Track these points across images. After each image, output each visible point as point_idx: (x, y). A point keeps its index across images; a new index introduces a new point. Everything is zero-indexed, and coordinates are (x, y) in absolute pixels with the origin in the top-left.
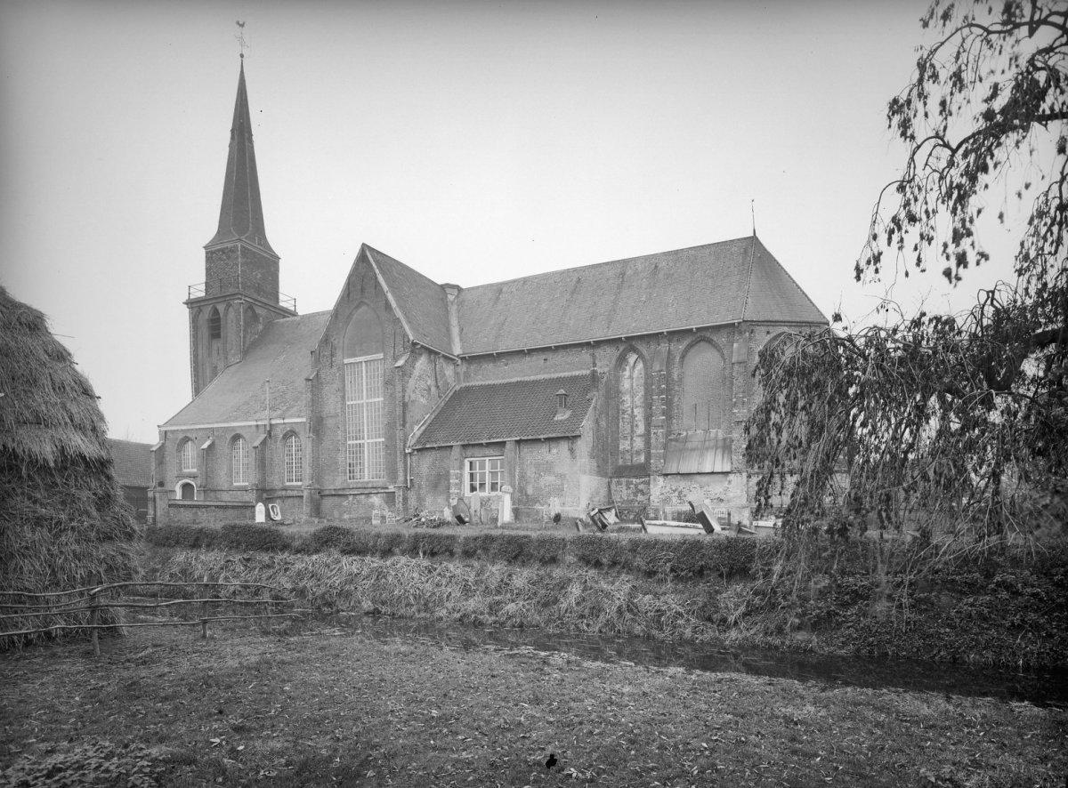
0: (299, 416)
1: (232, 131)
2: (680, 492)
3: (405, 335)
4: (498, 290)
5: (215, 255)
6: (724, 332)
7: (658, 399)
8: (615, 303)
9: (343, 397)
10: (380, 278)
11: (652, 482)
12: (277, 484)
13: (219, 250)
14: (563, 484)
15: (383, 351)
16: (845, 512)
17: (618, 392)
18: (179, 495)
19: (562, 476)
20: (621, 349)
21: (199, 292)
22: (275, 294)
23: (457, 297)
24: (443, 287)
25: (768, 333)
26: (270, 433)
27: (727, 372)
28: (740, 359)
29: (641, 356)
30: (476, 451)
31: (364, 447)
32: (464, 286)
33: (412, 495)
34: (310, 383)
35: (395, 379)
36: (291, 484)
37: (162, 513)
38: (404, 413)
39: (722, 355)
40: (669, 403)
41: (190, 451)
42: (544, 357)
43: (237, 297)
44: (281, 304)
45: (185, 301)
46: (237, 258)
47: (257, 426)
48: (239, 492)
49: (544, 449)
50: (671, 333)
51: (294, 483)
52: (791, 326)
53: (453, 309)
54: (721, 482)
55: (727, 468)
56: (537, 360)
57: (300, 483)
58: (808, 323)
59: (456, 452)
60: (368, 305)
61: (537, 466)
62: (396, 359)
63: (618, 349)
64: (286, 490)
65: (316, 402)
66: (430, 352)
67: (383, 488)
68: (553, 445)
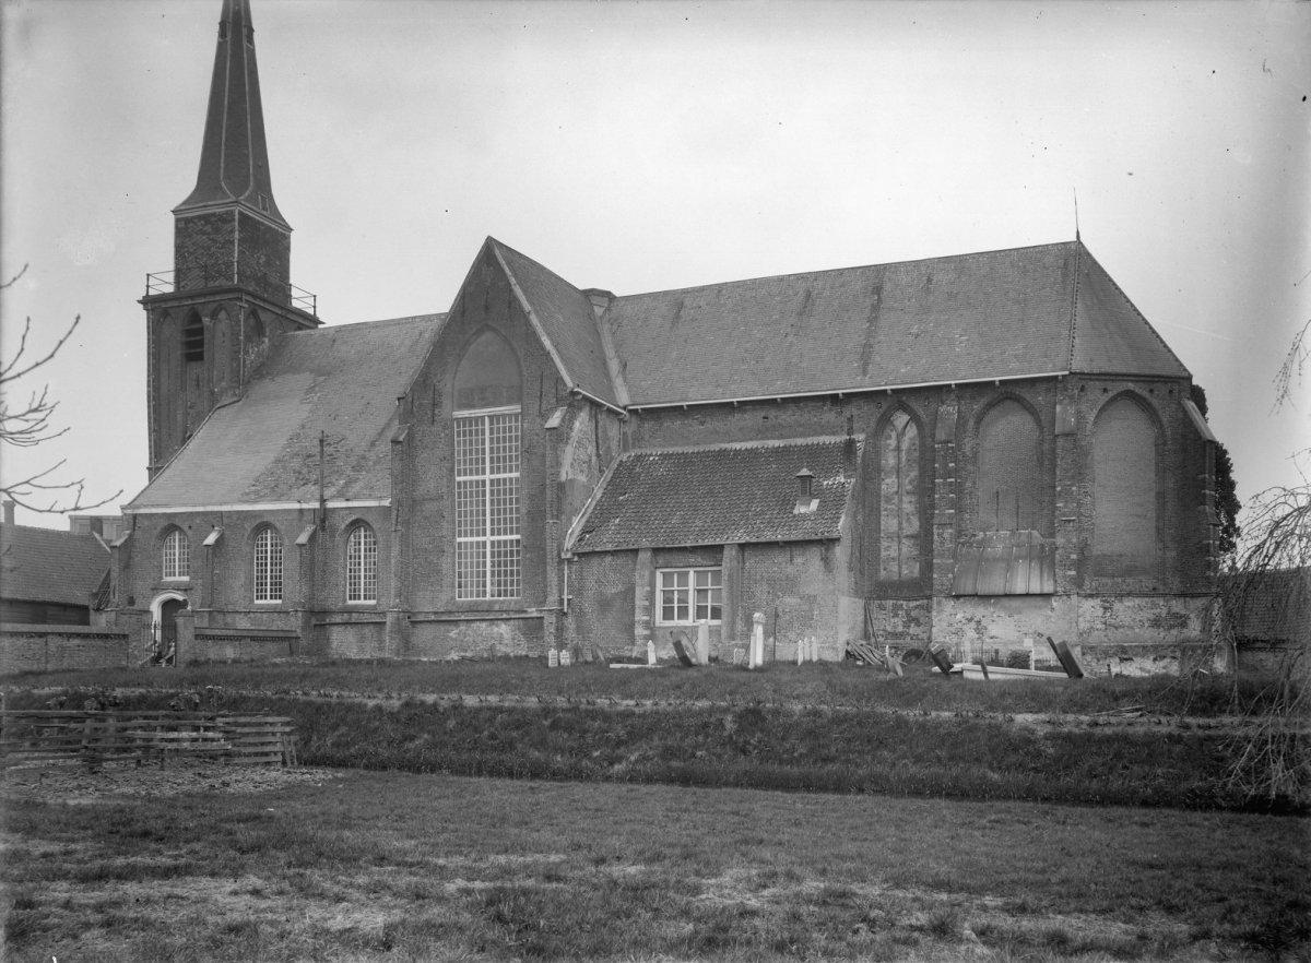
0: (370, 497)
2: (979, 622)
3: (559, 380)
4: (677, 303)
5: (193, 229)
6: (1042, 387)
7: (944, 484)
8: (870, 334)
9: (452, 470)
10: (518, 291)
11: (935, 606)
12: (331, 604)
13: (199, 217)
16: (831, 782)
17: (879, 470)
19: (811, 599)
20: (885, 406)
22: (284, 289)
23: (608, 309)
25: (1105, 390)
26: (323, 521)
27: (1046, 446)
28: (1067, 430)
29: (915, 418)
32: (617, 293)
33: (570, 622)
34: (399, 447)
35: (539, 452)
37: (187, 648)
38: (559, 498)
39: (1038, 421)
40: (958, 489)
41: (176, 547)
44: (296, 304)
46: (232, 231)
48: (265, 616)
49: (780, 558)
51: (362, 602)
52: (1137, 381)
53: (605, 328)
54: (1040, 608)
55: (1048, 588)
57: (373, 602)
58: (1163, 377)
59: (644, 557)
60: (494, 330)
61: (772, 582)
62: (544, 416)
64: (350, 612)
66: (594, 405)
68: (796, 552)
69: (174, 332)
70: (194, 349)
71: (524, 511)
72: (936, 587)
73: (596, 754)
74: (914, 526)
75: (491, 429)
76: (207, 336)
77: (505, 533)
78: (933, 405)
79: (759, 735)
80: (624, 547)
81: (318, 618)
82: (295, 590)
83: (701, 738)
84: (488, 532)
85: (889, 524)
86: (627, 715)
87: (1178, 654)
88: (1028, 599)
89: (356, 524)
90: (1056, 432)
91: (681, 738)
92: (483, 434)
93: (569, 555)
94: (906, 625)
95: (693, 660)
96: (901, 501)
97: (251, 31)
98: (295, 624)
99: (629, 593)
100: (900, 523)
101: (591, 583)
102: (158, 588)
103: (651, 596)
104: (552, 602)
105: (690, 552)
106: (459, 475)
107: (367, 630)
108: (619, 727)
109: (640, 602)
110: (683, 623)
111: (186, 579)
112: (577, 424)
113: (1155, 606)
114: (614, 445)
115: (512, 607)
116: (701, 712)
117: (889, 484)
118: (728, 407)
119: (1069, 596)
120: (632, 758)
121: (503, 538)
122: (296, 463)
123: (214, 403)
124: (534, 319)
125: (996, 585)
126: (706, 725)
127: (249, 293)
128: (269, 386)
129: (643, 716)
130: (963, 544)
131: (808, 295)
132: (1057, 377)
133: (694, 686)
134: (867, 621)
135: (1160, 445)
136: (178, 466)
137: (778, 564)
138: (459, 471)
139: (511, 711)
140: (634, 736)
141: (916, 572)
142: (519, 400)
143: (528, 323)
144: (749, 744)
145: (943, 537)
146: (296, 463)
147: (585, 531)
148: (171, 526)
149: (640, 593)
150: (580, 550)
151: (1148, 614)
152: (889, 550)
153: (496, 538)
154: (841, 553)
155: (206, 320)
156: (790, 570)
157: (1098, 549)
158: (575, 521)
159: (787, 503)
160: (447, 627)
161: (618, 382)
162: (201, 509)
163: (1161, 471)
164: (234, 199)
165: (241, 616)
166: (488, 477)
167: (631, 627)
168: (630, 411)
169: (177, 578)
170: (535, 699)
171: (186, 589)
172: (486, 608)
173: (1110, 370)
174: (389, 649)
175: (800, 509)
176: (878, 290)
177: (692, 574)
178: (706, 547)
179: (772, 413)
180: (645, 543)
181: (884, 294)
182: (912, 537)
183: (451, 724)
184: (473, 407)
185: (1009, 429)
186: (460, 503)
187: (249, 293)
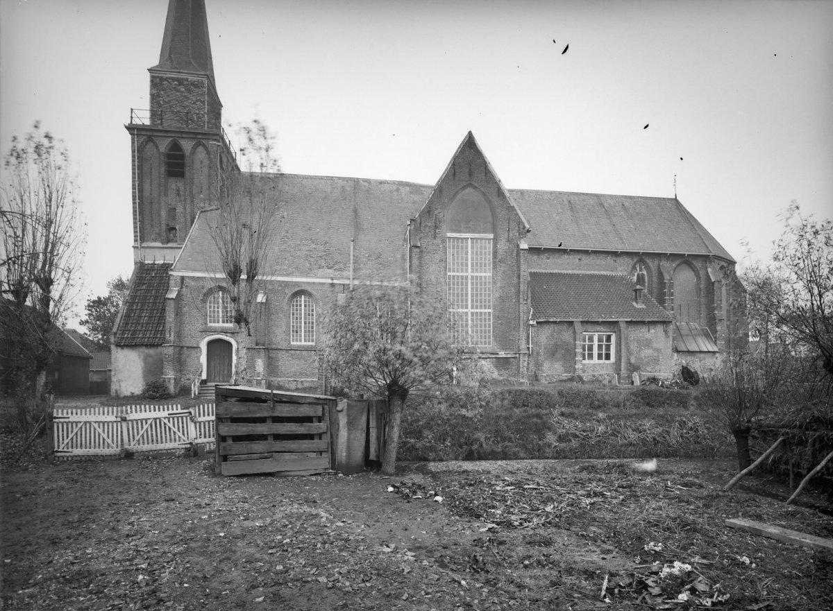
13: (174, 79)
14: (658, 356)
15: (494, 232)
19: (658, 350)
31: (223, 317)
39: (697, 275)
43: (215, 137)
47: (333, 285)
48: (304, 353)
49: (644, 329)
56: (574, 259)
60: (475, 187)
61: (638, 341)
67: (493, 354)
106: (450, 271)
110: (591, 362)
125: (693, 347)
138: (450, 269)
165: (284, 352)
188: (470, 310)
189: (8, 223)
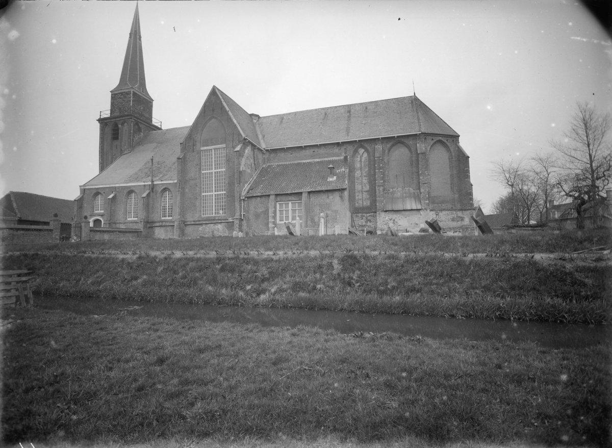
0: (171, 180)
1: (130, 34)
2: (394, 220)
3: (240, 134)
4: (281, 118)
5: (117, 97)
9: (200, 168)
12: (155, 219)
14: (336, 216)
17: (354, 169)
18: (91, 225)
19: (336, 212)
20: (356, 146)
21: (107, 114)
24: (252, 115)
25: (432, 139)
26: (153, 189)
28: (422, 152)
29: (366, 150)
30: (284, 198)
33: (244, 223)
34: (180, 160)
35: (232, 161)
36: (131, 219)
38: (240, 177)
39: (410, 150)
41: (100, 201)
42: (313, 150)
45: (97, 119)
46: (130, 97)
47: (145, 185)
48: (131, 224)
50: (383, 139)
51: (167, 218)
55: (419, 207)
59: (272, 197)
60: (216, 118)
62: (234, 148)
63: (354, 146)
65: (183, 172)
66: (253, 145)
68: (330, 194)
69: (109, 130)
70: (116, 135)
71: (227, 182)
72: (378, 208)
73: (249, 287)
74: (367, 188)
75: (215, 154)
76: (120, 131)
77: (220, 191)
78: (373, 146)
79: (357, 272)
80: (265, 194)
81: (150, 224)
82: (142, 215)
83: (318, 276)
84: (214, 191)
85: (358, 187)
86: (268, 261)
87: (461, 231)
88: (413, 212)
89: (165, 190)
90: (418, 153)
91: (305, 275)
92: (212, 155)
93: (244, 198)
94: (366, 222)
95: (295, 234)
96: (362, 179)
97: (140, 37)
98: (140, 227)
99: (266, 212)
100: (362, 187)
101: (252, 208)
102: (92, 216)
103: (275, 212)
104: (237, 216)
105: (290, 195)
106: (203, 170)
107: (168, 228)
108: (264, 269)
109: (271, 214)
111: (102, 211)
112: (246, 151)
113: (452, 214)
114: (260, 161)
115: (223, 218)
116: (315, 258)
117: (358, 174)
118: (301, 148)
119: (426, 210)
120: (273, 290)
121: (219, 193)
122: (146, 170)
123: (122, 153)
124: (230, 113)
126: (320, 267)
127: (135, 117)
128: (141, 148)
129: (279, 261)
130: (386, 193)
131: (326, 114)
132: (417, 134)
133: (306, 242)
134: (353, 221)
135: (450, 159)
136: (105, 173)
137: (323, 198)
138: (203, 169)
139: (198, 260)
140: (273, 275)
141: (369, 204)
142: (225, 143)
143: (228, 115)
144: (352, 278)
145: (379, 190)
146: (146, 170)
147: (249, 190)
148: (97, 193)
149: (271, 211)
150: (248, 196)
151: (451, 217)
152: (358, 196)
153: (217, 193)
154: (346, 193)
155: (120, 126)
156: (328, 201)
157: (433, 194)
158: (246, 186)
159: (324, 178)
160: (198, 226)
161: (262, 141)
162: (108, 186)
163: (451, 168)
164: (131, 87)
166: (214, 171)
167: (267, 224)
168: (266, 150)
169: (99, 211)
170: (214, 253)
171: (102, 215)
172: (213, 218)
173: (434, 132)
174: (175, 236)
175: (330, 179)
176: (349, 112)
177: (290, 203)
178: (296, 193)
179: (316, 150)
180: (272, 193)
181: (351, 113)
182: (367, 191)
183: (160, 269)
184: (208, 146)
185: (400, 154)
186: (203, 181)
187: (135, 117)
188: (214, 193)
189: (599, 169)
